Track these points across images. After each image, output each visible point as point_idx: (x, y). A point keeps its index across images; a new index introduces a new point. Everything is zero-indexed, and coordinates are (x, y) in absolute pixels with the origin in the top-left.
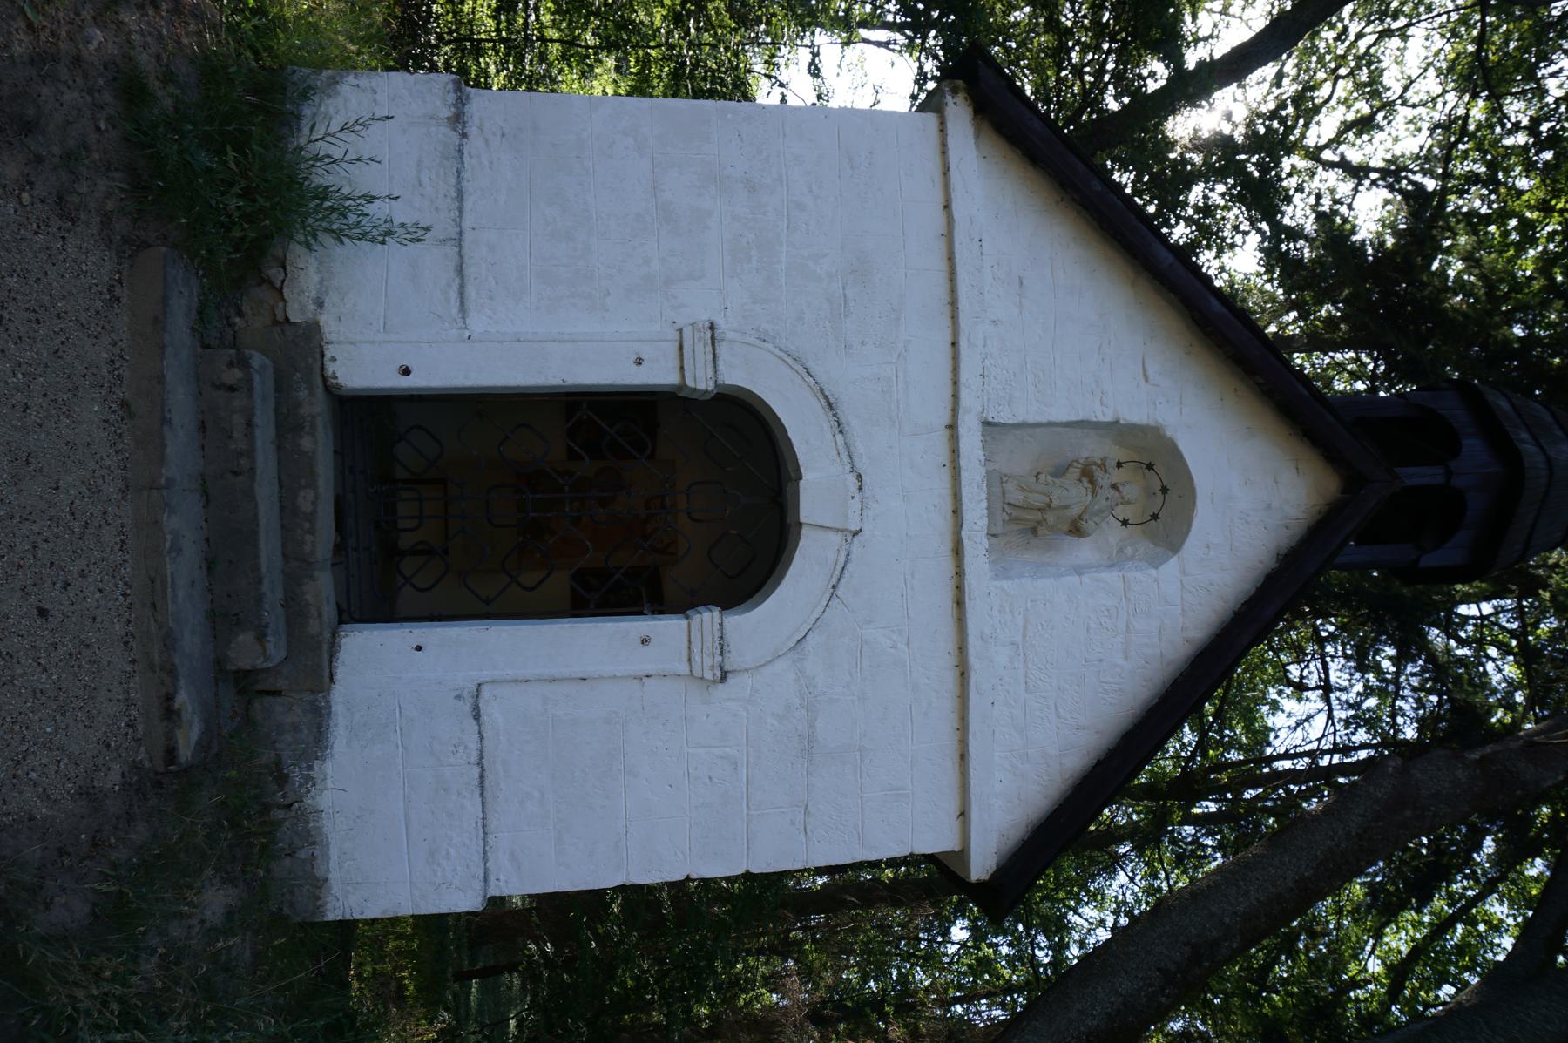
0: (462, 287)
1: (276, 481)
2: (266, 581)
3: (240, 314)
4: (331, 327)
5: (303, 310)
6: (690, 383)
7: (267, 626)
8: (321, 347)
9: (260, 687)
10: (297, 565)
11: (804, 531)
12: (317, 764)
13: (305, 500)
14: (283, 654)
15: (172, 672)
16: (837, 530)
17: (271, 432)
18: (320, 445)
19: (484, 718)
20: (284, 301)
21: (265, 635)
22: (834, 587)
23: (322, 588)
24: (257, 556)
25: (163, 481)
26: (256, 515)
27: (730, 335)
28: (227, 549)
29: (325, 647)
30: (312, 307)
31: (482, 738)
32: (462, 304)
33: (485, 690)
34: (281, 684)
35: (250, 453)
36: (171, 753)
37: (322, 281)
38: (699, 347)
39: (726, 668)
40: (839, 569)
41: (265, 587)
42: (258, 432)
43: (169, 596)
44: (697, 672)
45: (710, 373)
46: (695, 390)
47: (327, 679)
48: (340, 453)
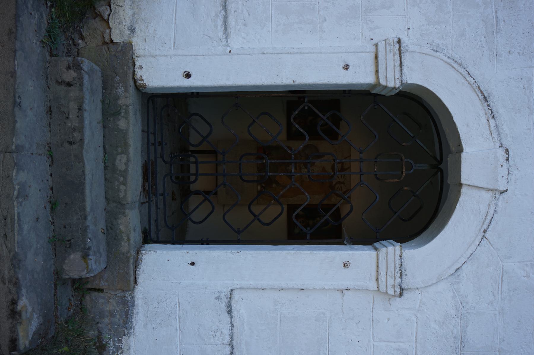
0: (226, 18)
1: (102, 148)
2: (89, 218)
3: (82, 38)
4: (140, 46)
5: (121, 34)
6: (383, 82)
7: (89, 249)
8: (133, 60)
9: (89, 286)
10: (114, 206)
11: (464, 190)
12: (124, 339)
13: (120, 162)
14: (103, 266)
15: (16, 284)
16: (489, 190)
17: (99, 115)
18: (132, 126)
19: (235, 313)
20: (110, 28)
21: (88, 255)
22: (485, 231)
23: (132, 222)
24: (84, 200)
25: (14, 147)
26: (83, 172)
27: (411, 48)
28: (64, 196)
29: (131, 261)
30: (127, 32)
31: (232, 326)
32: (226, 29)
33: (236, 295)
34: (103, 284)
35: (81, 129)
36: (14, 343)
37: (133, 15)
38: (390, 56)
39: (403, 287)
40: (489, 218)
41: (89, 222)
42: (86, 115)
43: (16, 229)
44: (383, 288)
45: (398, 75)
46: (386, 87)
47: (132, 283)
48: (146, 132)
